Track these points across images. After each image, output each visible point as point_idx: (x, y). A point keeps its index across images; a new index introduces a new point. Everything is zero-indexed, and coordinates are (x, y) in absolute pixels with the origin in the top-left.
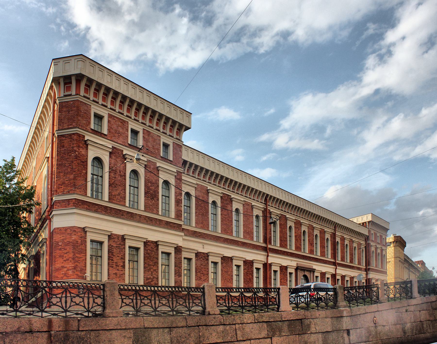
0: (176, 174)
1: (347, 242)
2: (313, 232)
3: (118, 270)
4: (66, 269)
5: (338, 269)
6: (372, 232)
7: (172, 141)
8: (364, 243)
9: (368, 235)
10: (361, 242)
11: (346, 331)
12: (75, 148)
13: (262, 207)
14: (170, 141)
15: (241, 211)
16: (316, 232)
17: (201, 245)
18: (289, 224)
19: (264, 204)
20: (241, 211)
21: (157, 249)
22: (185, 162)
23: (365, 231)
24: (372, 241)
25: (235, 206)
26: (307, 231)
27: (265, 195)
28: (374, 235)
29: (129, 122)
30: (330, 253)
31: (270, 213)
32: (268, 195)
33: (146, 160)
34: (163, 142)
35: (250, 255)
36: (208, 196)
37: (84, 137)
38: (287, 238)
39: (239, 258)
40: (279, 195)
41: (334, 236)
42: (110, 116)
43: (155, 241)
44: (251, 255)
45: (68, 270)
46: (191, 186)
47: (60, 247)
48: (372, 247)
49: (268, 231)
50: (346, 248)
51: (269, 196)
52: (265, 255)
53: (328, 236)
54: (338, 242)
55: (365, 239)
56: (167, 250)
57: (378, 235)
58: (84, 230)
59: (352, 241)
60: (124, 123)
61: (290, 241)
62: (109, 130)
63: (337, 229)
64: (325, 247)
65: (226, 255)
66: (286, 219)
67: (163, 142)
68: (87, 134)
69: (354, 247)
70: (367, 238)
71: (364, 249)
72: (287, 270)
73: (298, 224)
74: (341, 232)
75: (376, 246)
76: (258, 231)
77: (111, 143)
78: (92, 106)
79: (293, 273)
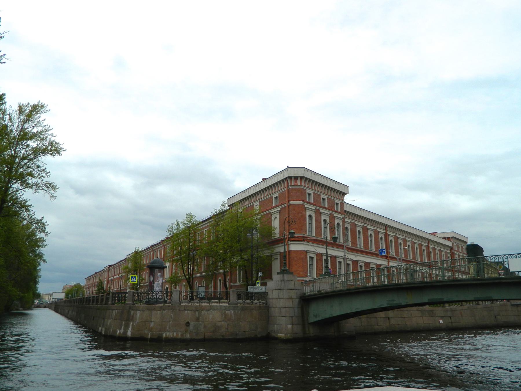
0: (374, 230)
1: (437, 252)
2: (414, 245)
3: (320, 272)
4: (299, 271)
5: (391, 262)
6: (455, 244)
7: (327, 197)
8: (450, 252)
9: (452, 246)
10: (448, 251)
11: (388, 318)
12: (301, 212)
13: (383, 232)
14: (338, 202)
15: (328, 222)
16: (416, 246)
17: (354, 256)
18: (400, 241)
19: (385, 230)
20: (328, 222)
21: (336, 260)
22: (345, 211)
23: (449, 244)
24: (455, 251)
25: (370, 232)
26: (373, 234)
27: (385, 225)
28: (457, 246)
29: (322, 195)
30: (426, 259)
31: (389, 235)
32: (387, 225)
33: (329, 213)
34: (336, 203)
35: (368, 260)
36: (356, 228)
37: (304, 205)
38: (399, 250)
39: (362, 261)
40: (427, 236)
41: (428, 247)
42: (314, 193)
43: (335, 255)
44: (380, 261)
45: (300, 272)
46: (360, 227)
47: (295, 260)
48: (456, 255)
49: (388, 245)
50: (437, 255)
51: (387, 226)
52: (387, 261)
53: (424, 248)
54: (431, 251)
55: (450, 249)
56: (312, 255)
57: (460, 246)
58: (306, 252)
59: (440, 251)
60: (320, 196)
61: (371, 244)
62: (328, 205)
63: (430, 243)
64: (422, 255)
65: (367, 261)
66: (398, 238)
67: (336, 203)
68: (321, 209)
69: (390, 241)
70: (451, 249)
71: (450, 256)
72: (370, 266)
73: (365, 230)
74: (441, 247)
75: (463, 255)
76: (338, 234)
77: (315, 207)
78: (307, 190)
79: (342, 262)
